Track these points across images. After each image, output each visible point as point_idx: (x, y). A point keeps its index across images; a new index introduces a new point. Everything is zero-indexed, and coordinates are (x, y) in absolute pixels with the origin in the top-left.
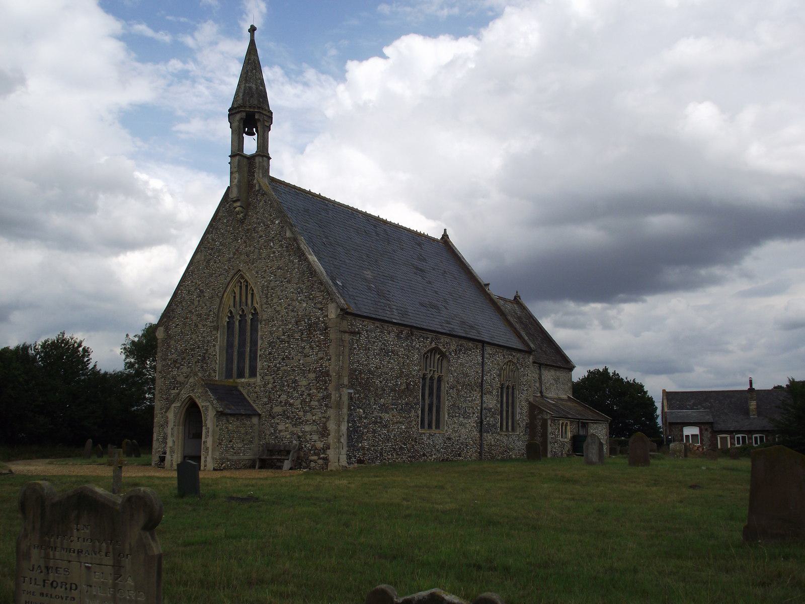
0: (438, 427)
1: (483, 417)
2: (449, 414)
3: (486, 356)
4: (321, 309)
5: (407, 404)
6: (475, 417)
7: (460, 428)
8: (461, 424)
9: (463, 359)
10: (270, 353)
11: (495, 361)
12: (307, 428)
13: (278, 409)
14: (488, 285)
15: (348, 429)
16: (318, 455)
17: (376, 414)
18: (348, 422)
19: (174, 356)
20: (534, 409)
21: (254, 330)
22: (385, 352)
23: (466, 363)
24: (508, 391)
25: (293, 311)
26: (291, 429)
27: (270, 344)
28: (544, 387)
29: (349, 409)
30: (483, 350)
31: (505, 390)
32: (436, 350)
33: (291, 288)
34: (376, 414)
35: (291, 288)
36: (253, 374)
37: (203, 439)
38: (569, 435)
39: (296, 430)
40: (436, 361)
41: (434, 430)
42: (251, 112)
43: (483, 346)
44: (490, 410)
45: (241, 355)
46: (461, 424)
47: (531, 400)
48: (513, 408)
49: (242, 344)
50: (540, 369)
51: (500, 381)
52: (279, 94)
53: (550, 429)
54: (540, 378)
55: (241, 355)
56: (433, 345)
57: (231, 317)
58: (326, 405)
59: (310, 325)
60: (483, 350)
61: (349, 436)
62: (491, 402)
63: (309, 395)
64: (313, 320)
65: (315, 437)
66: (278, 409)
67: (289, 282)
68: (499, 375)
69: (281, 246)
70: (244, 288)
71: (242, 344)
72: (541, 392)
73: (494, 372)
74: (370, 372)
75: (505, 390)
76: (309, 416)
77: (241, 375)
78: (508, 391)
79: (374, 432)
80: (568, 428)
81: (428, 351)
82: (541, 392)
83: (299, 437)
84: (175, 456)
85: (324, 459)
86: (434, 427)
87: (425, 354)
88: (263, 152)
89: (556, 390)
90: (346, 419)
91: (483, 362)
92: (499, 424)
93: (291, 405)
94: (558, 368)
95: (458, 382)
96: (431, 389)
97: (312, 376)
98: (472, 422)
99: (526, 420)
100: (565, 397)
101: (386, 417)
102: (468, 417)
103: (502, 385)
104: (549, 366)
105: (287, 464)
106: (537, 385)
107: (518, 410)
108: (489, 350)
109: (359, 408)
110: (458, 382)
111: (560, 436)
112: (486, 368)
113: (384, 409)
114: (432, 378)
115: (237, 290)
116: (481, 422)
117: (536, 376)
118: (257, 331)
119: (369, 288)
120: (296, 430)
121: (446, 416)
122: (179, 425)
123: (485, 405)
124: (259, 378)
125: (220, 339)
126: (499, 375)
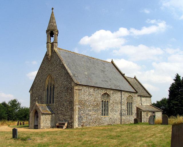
0: (107, 115)
1: (122, 112)
2: (110, 111)
3: (122, 94)
4: (70, 84)
5: (97, 109)
6: (119, 112)
7: (114, 115)
8: (115, 114)
9: (115, 95)
10: (57, 96)
11: (125, 96)
12: (67, 117)
13: (59, 112)
14: (124, 74)
15: (78, 117)
16: (70, 124)
17: (87, 112)
18: (78, 115)
19: (34, 98)
20: (138, 109)
21: (53, 90)
22: (90, 94)
23: (115, 97)
24: (129, 105)
25: (63, 84)
26: (63, 117)
27: (57, 94)
28: (142, 103)
29: (78, 111)
30: (121, 93)
31: (129, 104)
32: (106, 94)
33: (62, 78)
34: (87, 112)
35: (62, 78)
36: (53, 103)
37: (39, 121)
38: (149, 116)
39: (64, 118)
40: (106, 96)
41: (106, 116)
42: (51, 33)
43: (121, 92)
44: (124, 110)
45: (50, 97)
46: (115, 114)
47: (137, 106)
48: (131, 109)
49: (51, 95)
50: (141, 97)
51: (127, 101)
52: (60, 26)
53: (142, 114)
54: (141, 100)
55: (50, 97)
56: (105, 92)
57: (48, 87)
58: (72, 111)
59: (67, 88)
60: (121, 93)
61: (79, 119)
62: (124, 107)
63: (67, 108)
64: (68, 87)
65: (69, 119)
66: (59, 112)
67: (62, 76)
68: (127, 100)
69: (60, 67)
70: (51, 78)
71: (51, 95)
72: (141, 104)
73: (125, 99)
74: (86, 101)
75: (129, 104)
76: (67, 114)
77: (50, 103)
78: (129, 105)
79: (87, 117)
80: (149, 114)
81: (104, 94)
82: (141, 104)
83: (65, 119)
84: (32, 125)
85: (71, 125)
86: (106, 115)
87: (103, 95)
88: (56, 42)
89: (145, 103)
90: (77, 114)
91: (121, 96)
92: (127, 114)
93: (63, 111)
94: (146, 97)
95: (113, 102)
96: (105, 104)
97: (68, 102)
98: (118, 114)
99: (136, 112)
100: (149, 105)
101: (90, 113)
102: (117, 112)
103: (128, 102)
104: (144, 96)
105: (65, 127)
106: (140, 102)
107: (133, 109)
108: (123, 93)
109: (81, 111)
110: (113, 102)
111: (145, 117)
112: (122, 98)
113: (90, 111)
114: (105, 101)
115: (49, 80)
116: (121, 113)
117: (140, 99)
118: (54, 90)
119: (86, 77)
120: (64, 118)
121: (110, 112)
122: (33, 117)
123: (122, 108)
124: (55, 103)
125: (45, 93)
126: (127, 100)
